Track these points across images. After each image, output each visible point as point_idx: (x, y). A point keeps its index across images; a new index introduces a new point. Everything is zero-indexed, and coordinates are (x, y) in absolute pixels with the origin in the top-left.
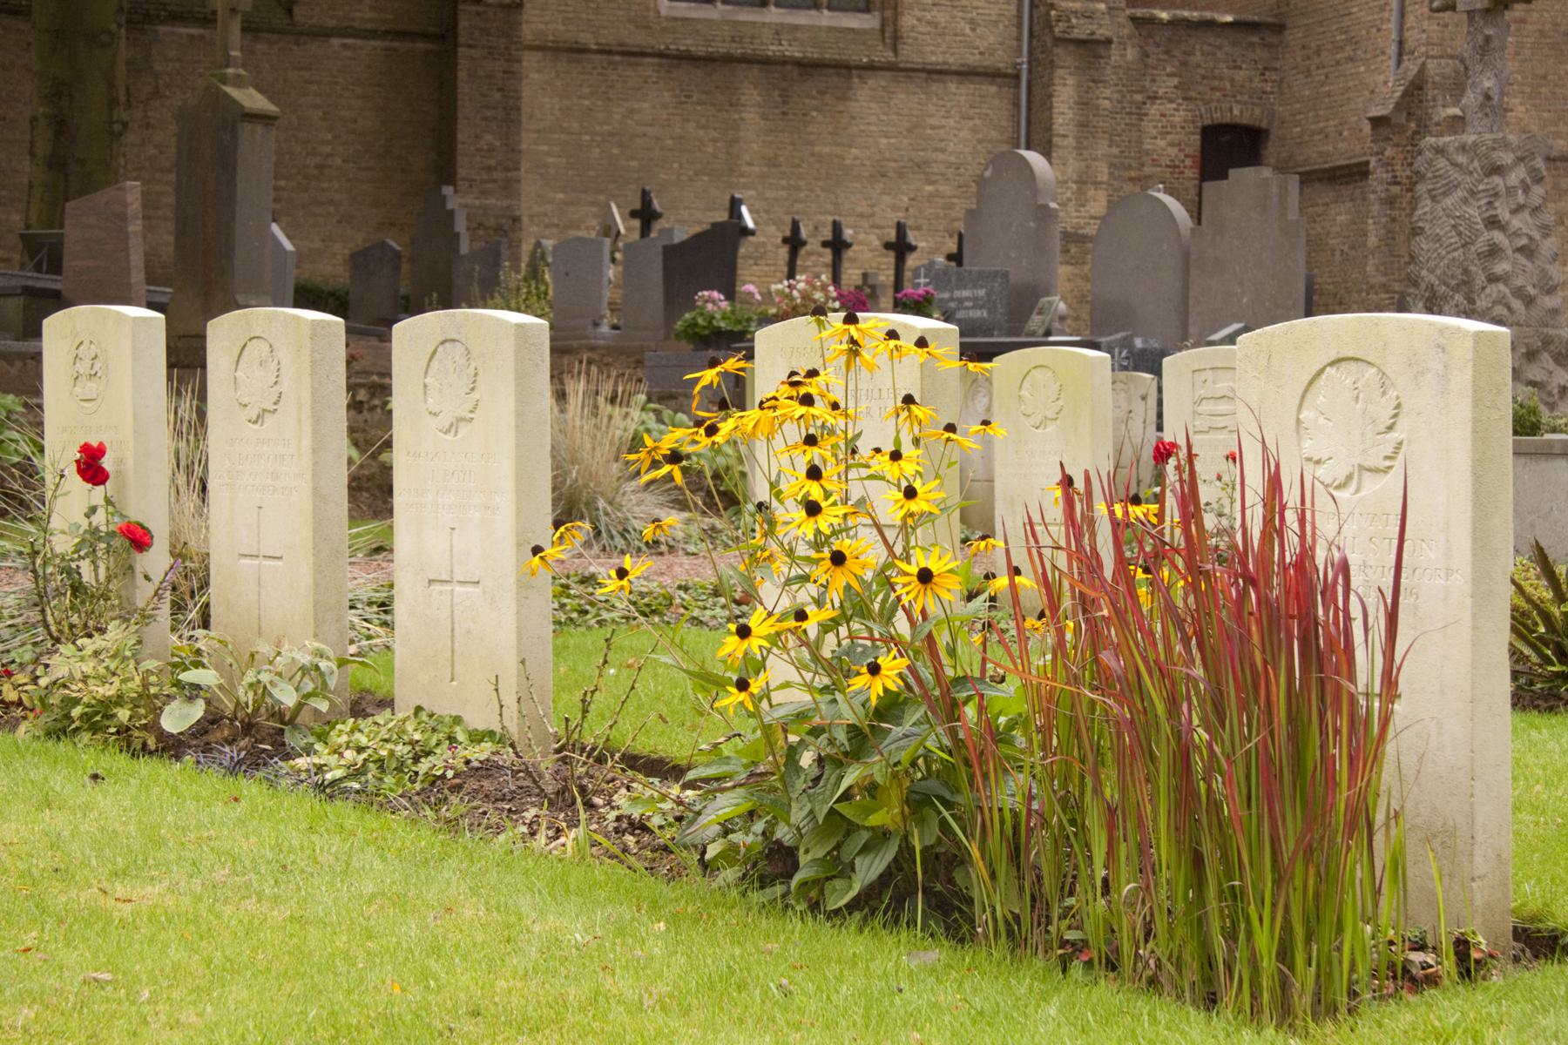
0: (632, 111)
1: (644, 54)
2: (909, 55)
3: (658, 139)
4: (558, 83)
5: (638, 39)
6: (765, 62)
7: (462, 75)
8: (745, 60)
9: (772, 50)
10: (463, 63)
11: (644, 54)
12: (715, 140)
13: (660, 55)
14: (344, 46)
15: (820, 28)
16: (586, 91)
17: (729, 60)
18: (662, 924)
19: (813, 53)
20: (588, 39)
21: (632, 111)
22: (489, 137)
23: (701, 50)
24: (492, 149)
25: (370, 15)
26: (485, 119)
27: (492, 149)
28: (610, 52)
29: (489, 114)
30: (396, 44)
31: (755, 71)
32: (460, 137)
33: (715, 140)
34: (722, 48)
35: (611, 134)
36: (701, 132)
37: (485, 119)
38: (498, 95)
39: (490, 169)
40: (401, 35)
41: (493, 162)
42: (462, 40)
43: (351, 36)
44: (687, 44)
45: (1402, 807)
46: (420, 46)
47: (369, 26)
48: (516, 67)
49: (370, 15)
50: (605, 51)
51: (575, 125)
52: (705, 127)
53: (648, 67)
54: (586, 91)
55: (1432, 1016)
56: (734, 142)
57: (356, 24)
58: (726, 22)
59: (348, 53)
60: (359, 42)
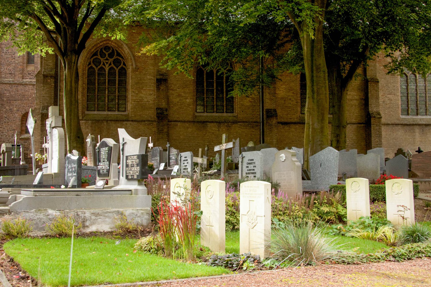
0: (397, 134)
1: (399, 124)
2: (53, 72)
3: (401, 138)
4: (385, 130)
5: (397, 122)
6: (419, 125)
7: (372, 129)
8: (416, 125)
9: (420, 123)
10: (372, 127)
11: (399, 124)
12: (411, 138)
13: (401, 124)
14: (350, 126)
15: (427, 119)
16: (389, 131)
17: (413, 125)
18: (14, 276)
19: (427, 123)
20: (389, 122)
21: (397, 134)
22: (377, 139)
23: (408, 123)
24: (377, 141)
25: (354, 121)
26: (376, 136)
27: (377, 141)
28: (393, 124)
29: (377, 136)
30: (359, 125)
31: (418, 126)
32: (372, 140)
33: (411, 138)
34: (412, 123)
35: (394, 138)
36: (409, 137)
37: (376, 136)
38: (378, 132)
39: (377, 145)
40: (359, 123)
41: (377, 144)
42: (372, 124)
43: (352, 124)
44: (406, 122)
45: (428, 241)
46: (362, 125)
47: (354, 122)
48: (381, 128)
49: (354, 121)
50: (393, 124)
51: (388, 137)
52: (409, 136)
53: (400, 127)
54: (389, 131)
55: (345, 283)
56: (414, 138)
57: (352, 122)
58: (412, 118)
59: (351, 127)
60: (353, 125)
